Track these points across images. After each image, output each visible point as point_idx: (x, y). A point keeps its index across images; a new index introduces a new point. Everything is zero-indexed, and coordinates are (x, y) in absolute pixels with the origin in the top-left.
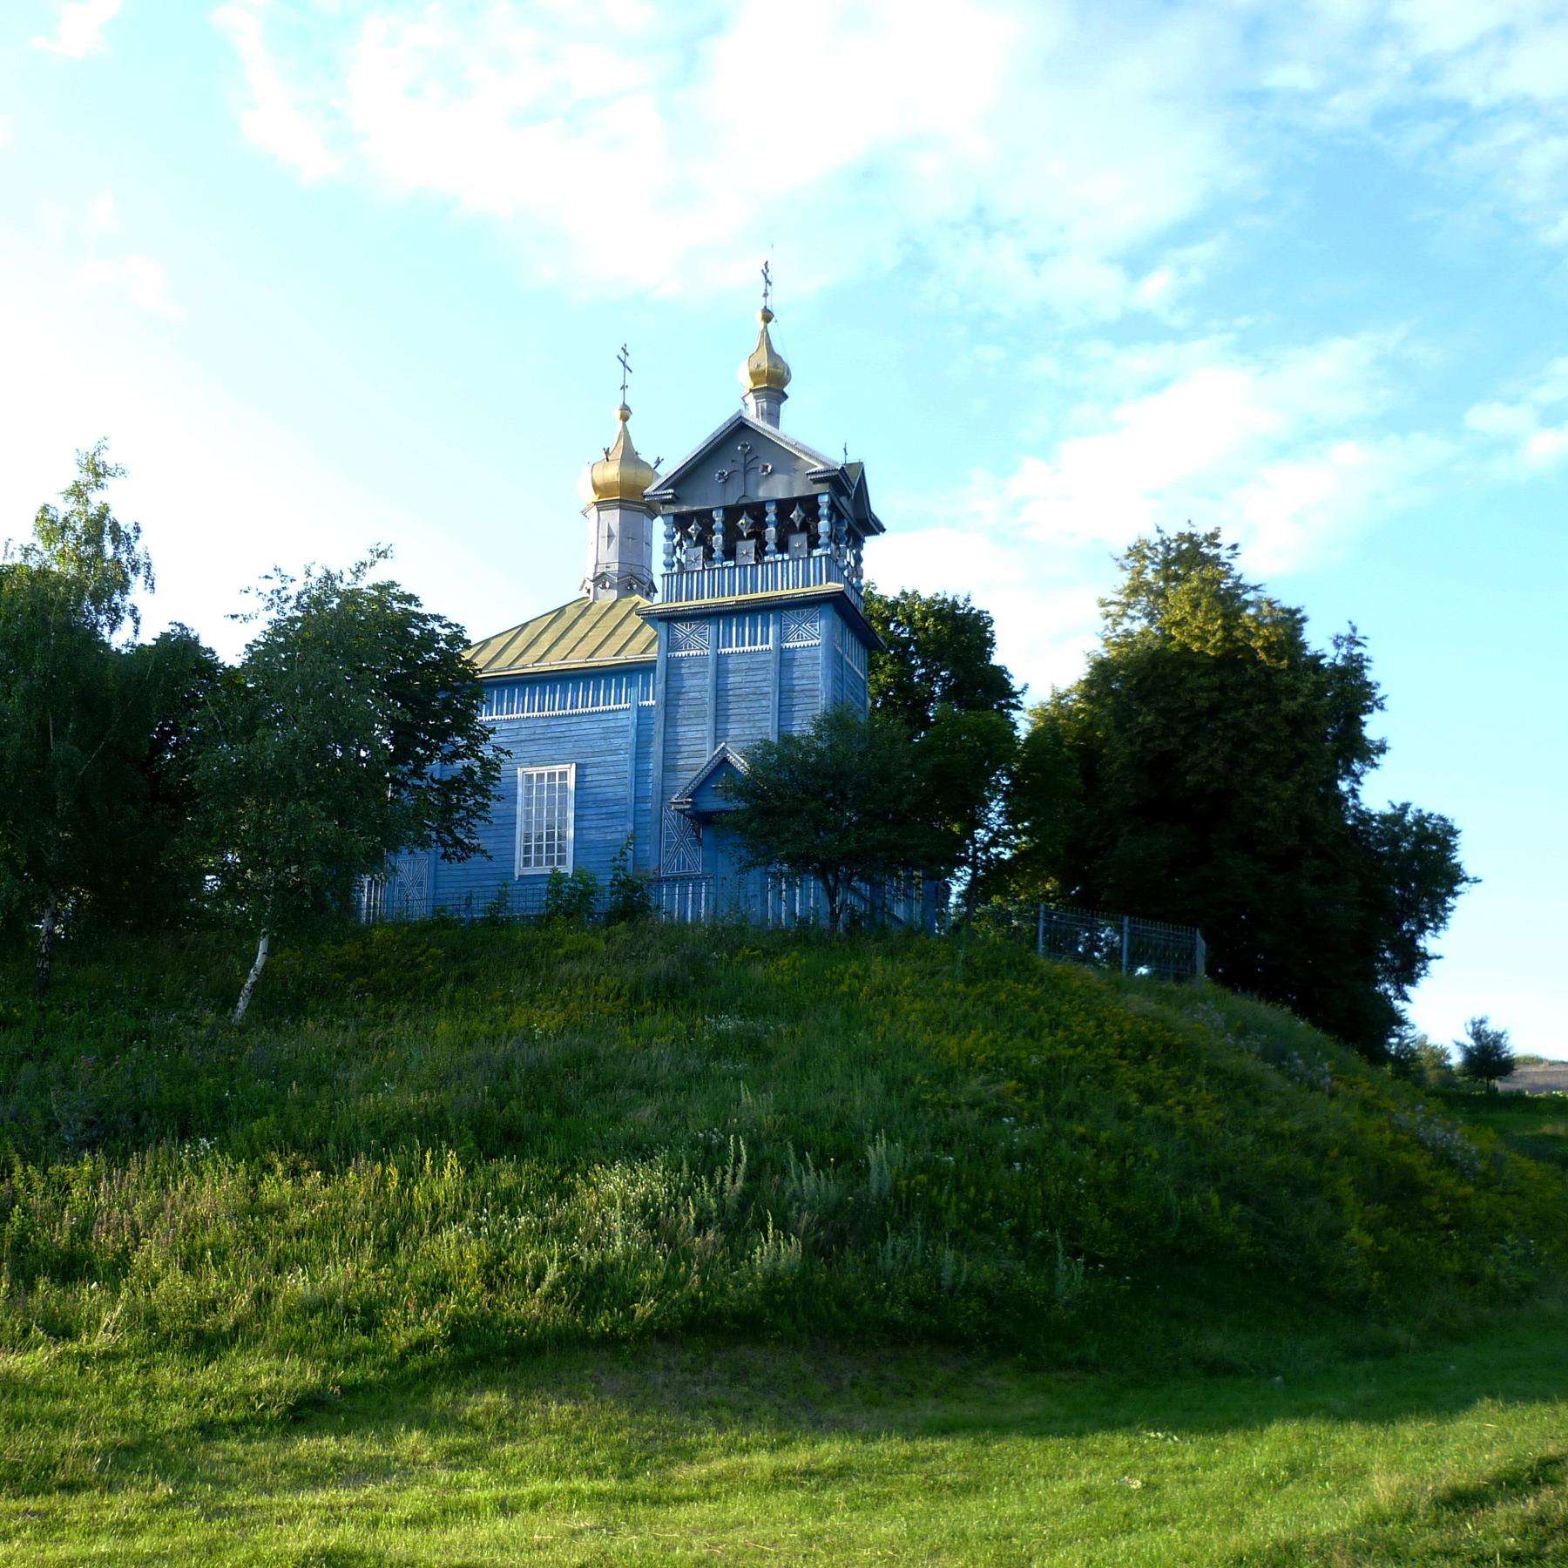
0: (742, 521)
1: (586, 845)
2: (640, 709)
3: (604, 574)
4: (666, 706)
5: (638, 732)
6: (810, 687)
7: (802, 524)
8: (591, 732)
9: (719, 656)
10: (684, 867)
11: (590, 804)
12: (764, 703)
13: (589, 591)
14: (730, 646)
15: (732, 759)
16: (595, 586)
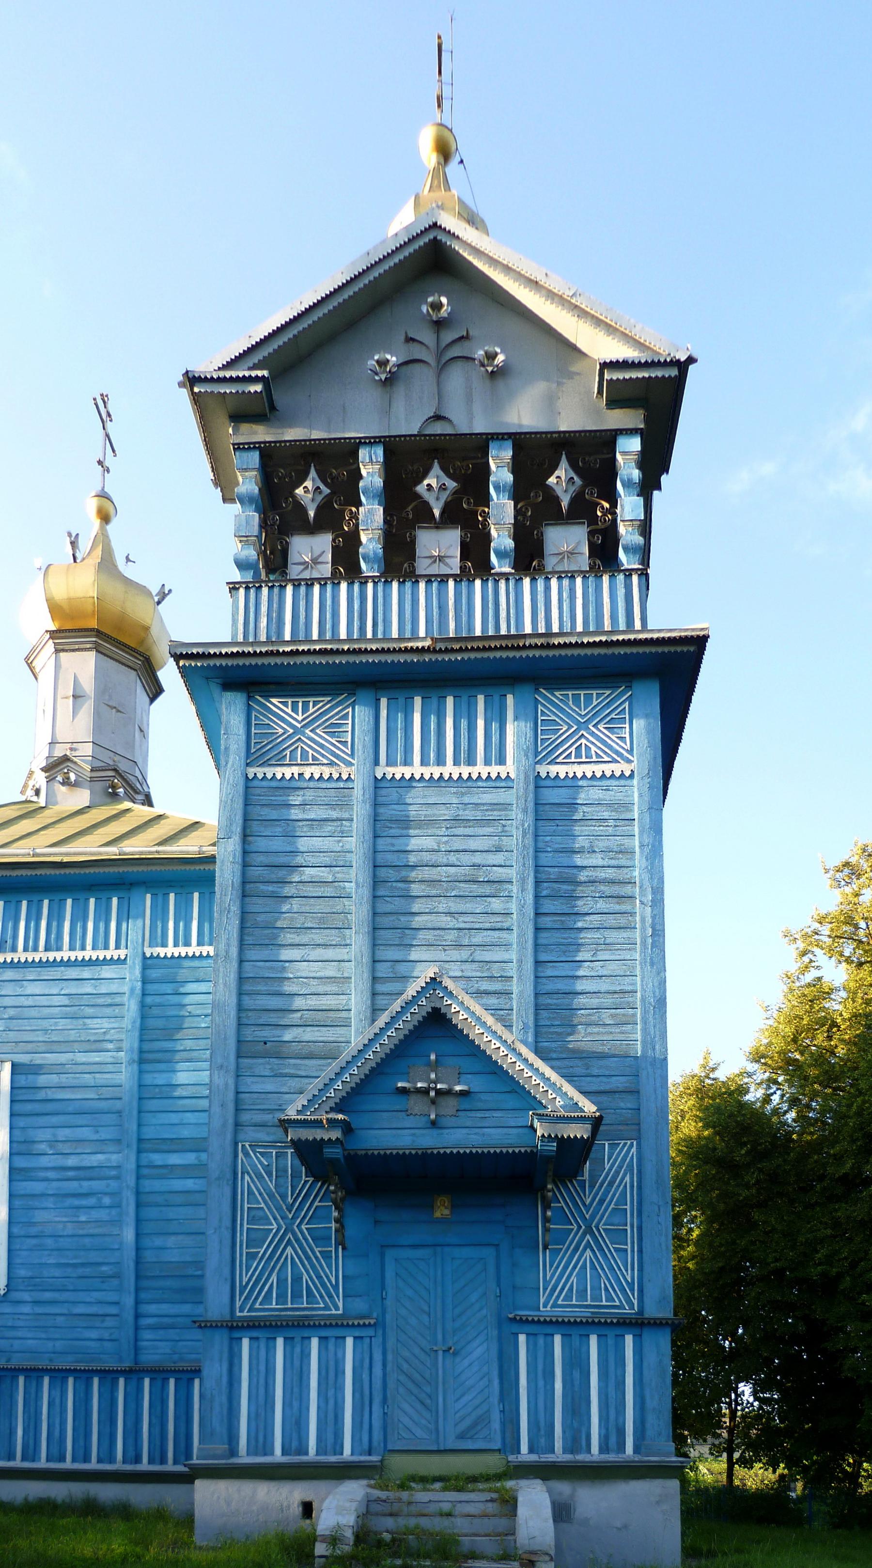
0: (431, 480)
1: (33, 1230)
2: (148, 962)
3: (66, 759)
4: (244, 895)
5: (143, 1006)
6: (610, 873)
7: (573, 501)
8: (43, 1001)
9: (378, 783)
10: (296, 1296)
11: (43, 1147)
12: (496, 905)
13: (37, 792)
14: (407, 762)
15: (459, 1016)
16: (50, 780)
